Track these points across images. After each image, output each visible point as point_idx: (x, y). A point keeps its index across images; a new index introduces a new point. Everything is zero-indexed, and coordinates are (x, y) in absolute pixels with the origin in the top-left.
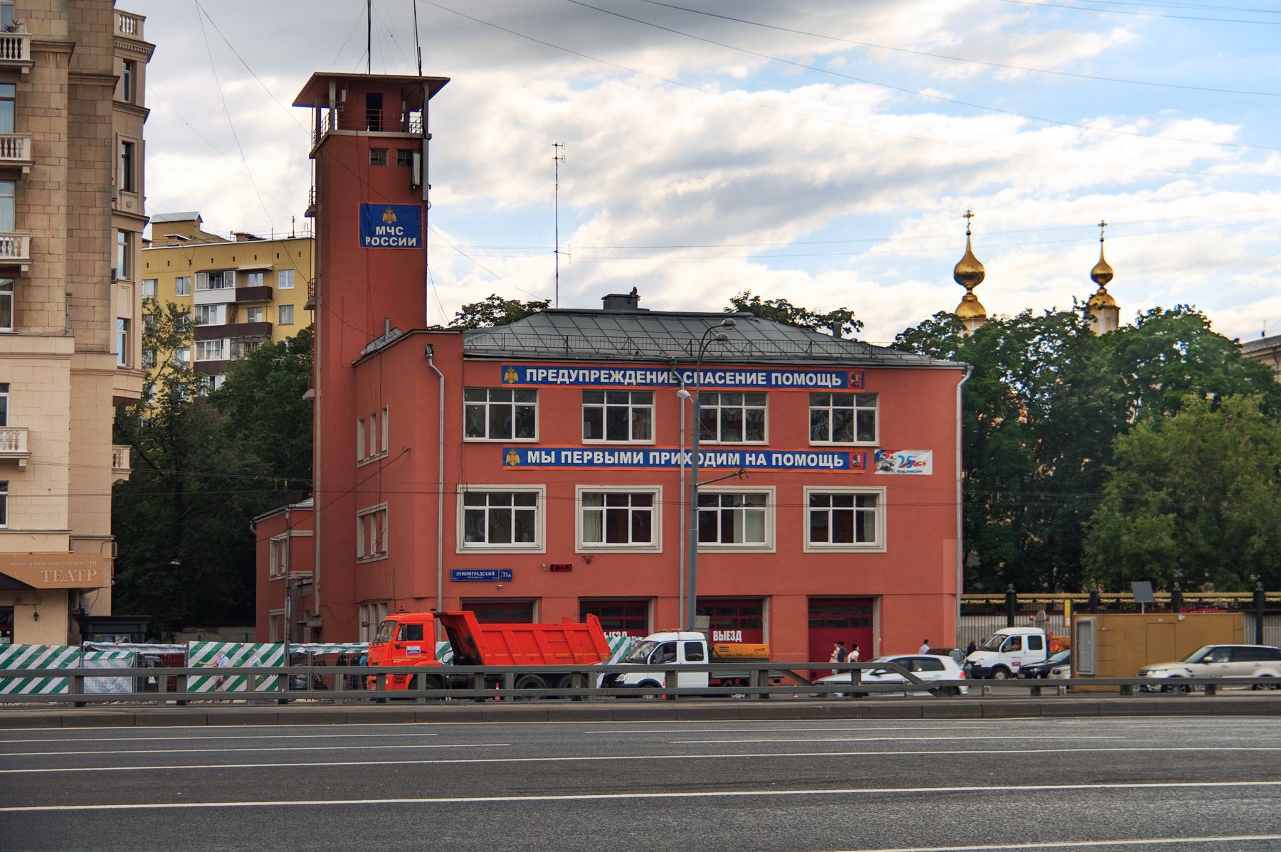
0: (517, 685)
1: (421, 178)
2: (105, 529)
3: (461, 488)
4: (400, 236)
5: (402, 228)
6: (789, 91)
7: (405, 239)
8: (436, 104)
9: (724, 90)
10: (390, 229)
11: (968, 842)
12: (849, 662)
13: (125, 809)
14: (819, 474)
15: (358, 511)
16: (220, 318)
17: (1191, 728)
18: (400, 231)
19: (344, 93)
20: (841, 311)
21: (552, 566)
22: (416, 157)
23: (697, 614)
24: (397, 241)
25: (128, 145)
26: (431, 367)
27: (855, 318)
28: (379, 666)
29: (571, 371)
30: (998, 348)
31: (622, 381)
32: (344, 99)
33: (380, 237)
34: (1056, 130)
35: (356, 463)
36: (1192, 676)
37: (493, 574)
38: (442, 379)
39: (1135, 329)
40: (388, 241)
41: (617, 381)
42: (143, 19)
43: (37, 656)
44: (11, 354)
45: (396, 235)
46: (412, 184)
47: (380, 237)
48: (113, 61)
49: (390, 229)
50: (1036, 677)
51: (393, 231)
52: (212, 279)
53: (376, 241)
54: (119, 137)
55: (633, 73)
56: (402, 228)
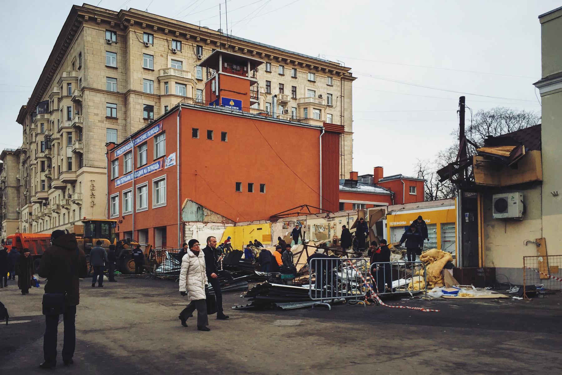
0: (537, 85)
2: (465, 108)
6: (530, 181)
9: (83, 31)
11: (242, 74)
12: (341, 201)
13: (328, 278)
14: (36, 151)
15: (123, 191)
16: (146, 137)
17: (511, 345)
20: (347, 69)
21: (249, 191)
23: (44, 180)
25: (26, 133)
27: (258, 83)
28: (60, 119)
30: (243, 257)
34: (422, 340)
35: (318, 275)
36: (401, 340)
38: (404, 185)
39: (41, 98)
42: (292, 77)
44: (259, 45)
46: (211, 90)
48: (347, 132)
50: (90, 17)
52: (199, 208)
54: (306, 87)
55: (116, 293)
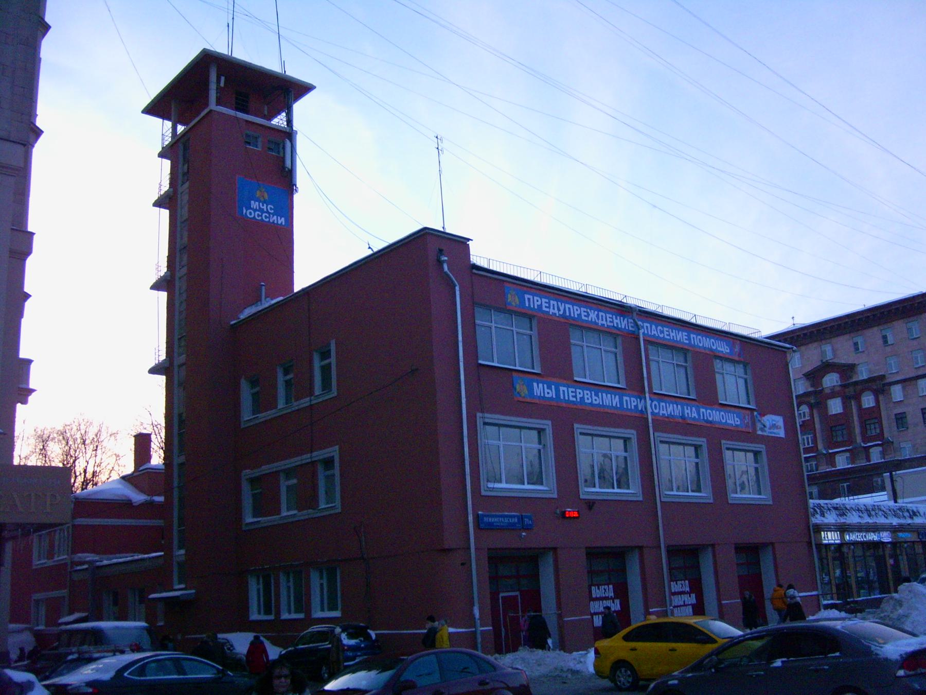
1: (292, 164)
3: (247, 473)
4: (272, 214)
5: (272, 207)
7: (275, 217)
8: (299, 107)
10: (263, 206)
18: (271, 209)
19: (223, 79)
22: (288, 143)
24: (269, 218)
26: (446, 273)
29: (559, 303)
31: (597, 321)
32: (222, 84)
33: (255, 210)
37: (516, 520)
38: (457, 288)
40: (261, 216)
41: (593, 320)
43: (323, 599)
45: (267, 212)
46: (284, 167)
47: (255, 210)
49: (263, 206)
51: (265, 207)
53: (250, 214)
56: (272, 207)
